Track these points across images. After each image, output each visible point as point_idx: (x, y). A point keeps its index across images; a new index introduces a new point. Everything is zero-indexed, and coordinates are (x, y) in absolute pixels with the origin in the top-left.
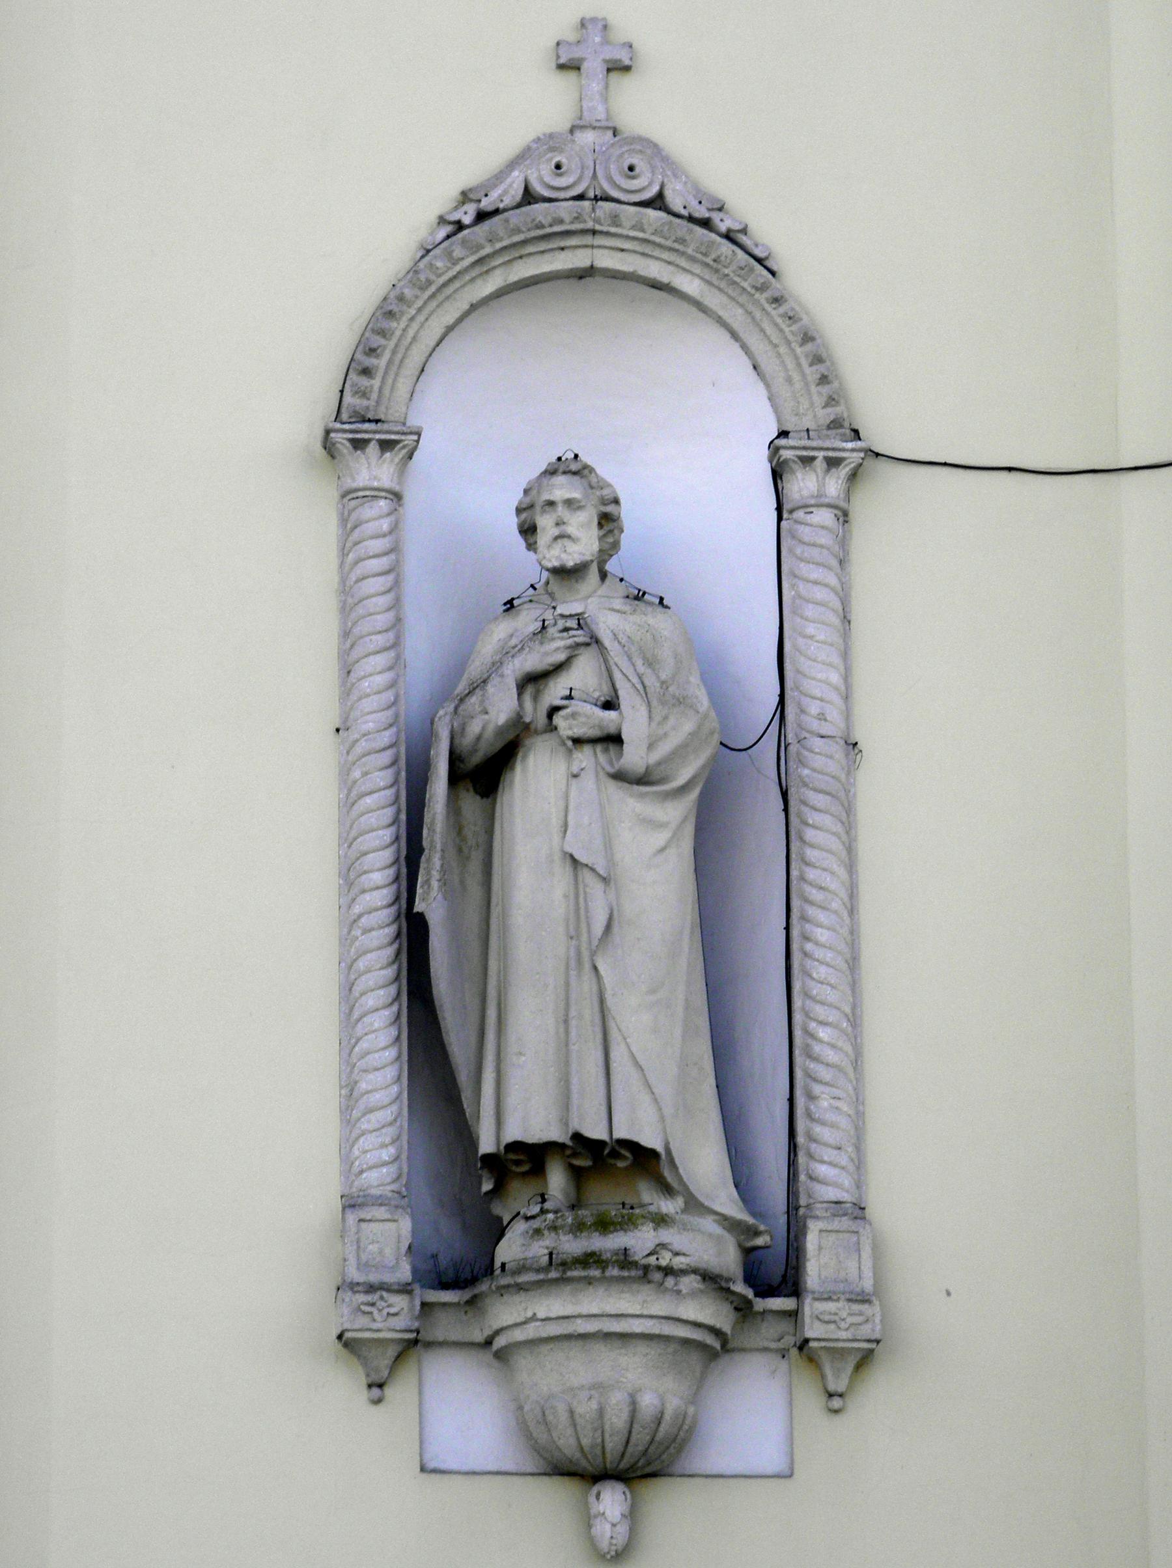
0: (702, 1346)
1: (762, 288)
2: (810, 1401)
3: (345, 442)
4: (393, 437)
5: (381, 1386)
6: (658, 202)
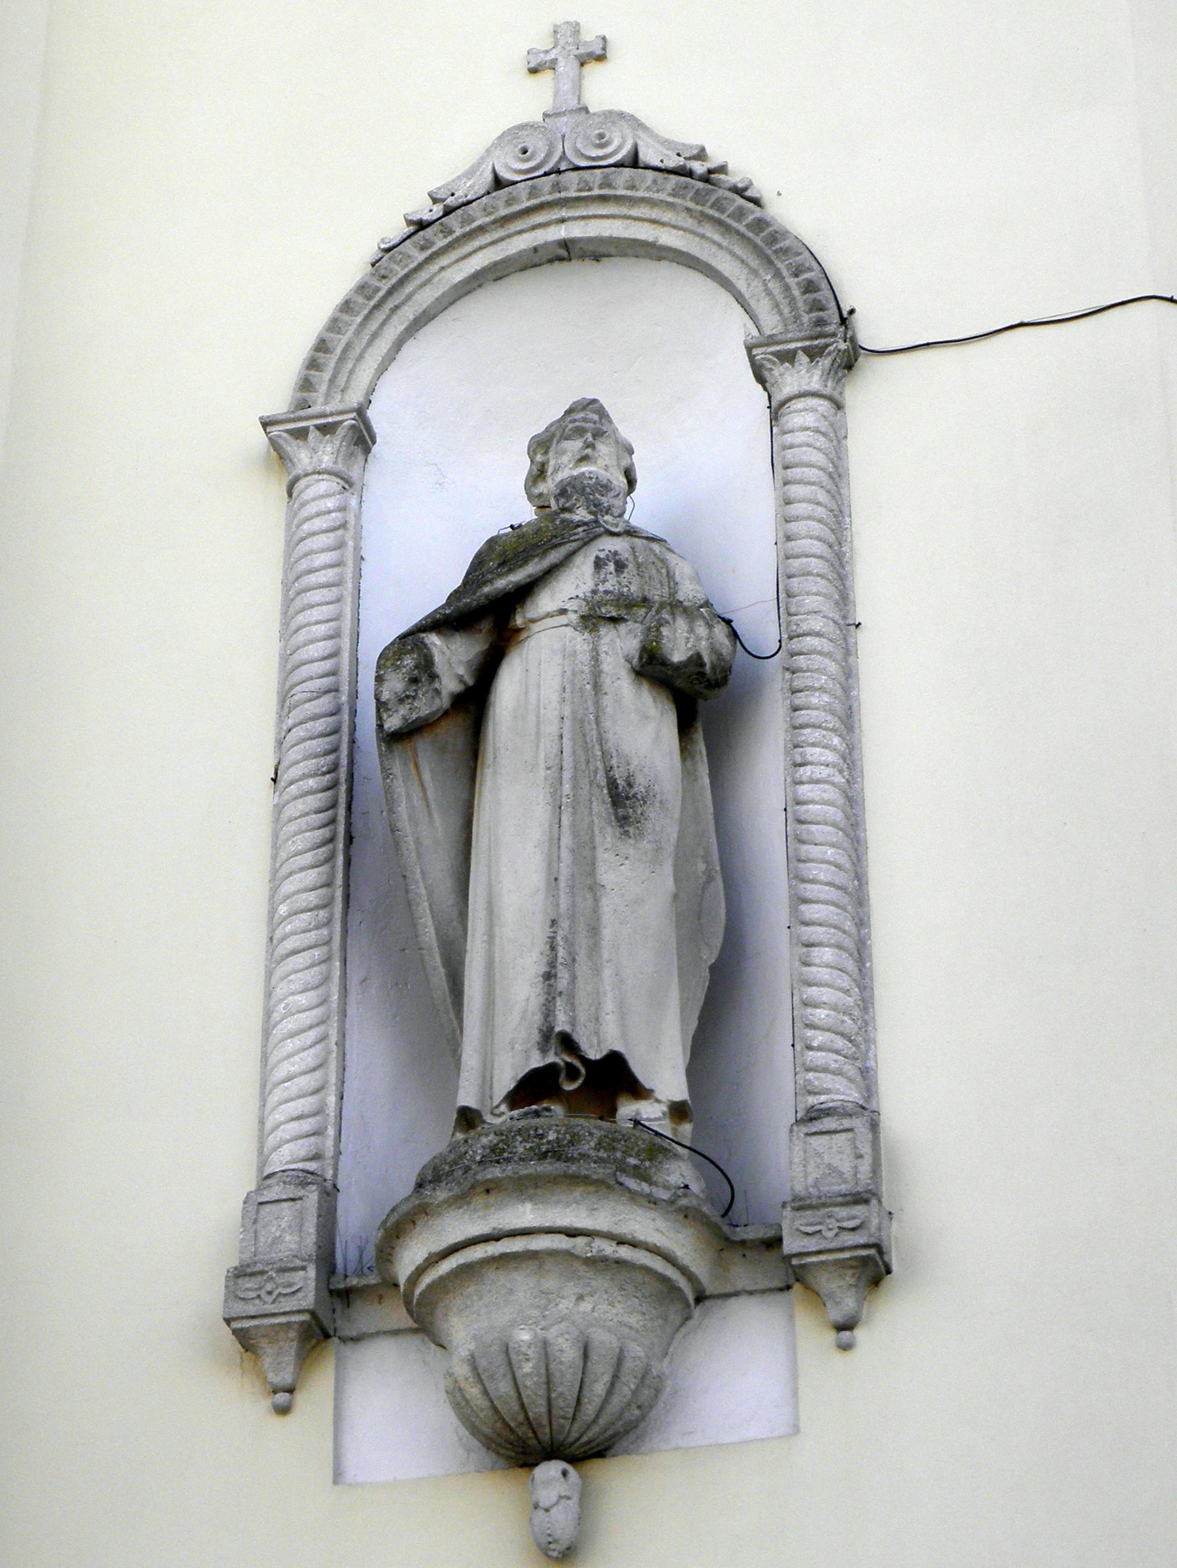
0: (669, 1289)
1: (740, 214)
2: (814, 1338)
3: (285, 435)
4: (330, 420)
5: (291, 1390)
6: (634, 161)
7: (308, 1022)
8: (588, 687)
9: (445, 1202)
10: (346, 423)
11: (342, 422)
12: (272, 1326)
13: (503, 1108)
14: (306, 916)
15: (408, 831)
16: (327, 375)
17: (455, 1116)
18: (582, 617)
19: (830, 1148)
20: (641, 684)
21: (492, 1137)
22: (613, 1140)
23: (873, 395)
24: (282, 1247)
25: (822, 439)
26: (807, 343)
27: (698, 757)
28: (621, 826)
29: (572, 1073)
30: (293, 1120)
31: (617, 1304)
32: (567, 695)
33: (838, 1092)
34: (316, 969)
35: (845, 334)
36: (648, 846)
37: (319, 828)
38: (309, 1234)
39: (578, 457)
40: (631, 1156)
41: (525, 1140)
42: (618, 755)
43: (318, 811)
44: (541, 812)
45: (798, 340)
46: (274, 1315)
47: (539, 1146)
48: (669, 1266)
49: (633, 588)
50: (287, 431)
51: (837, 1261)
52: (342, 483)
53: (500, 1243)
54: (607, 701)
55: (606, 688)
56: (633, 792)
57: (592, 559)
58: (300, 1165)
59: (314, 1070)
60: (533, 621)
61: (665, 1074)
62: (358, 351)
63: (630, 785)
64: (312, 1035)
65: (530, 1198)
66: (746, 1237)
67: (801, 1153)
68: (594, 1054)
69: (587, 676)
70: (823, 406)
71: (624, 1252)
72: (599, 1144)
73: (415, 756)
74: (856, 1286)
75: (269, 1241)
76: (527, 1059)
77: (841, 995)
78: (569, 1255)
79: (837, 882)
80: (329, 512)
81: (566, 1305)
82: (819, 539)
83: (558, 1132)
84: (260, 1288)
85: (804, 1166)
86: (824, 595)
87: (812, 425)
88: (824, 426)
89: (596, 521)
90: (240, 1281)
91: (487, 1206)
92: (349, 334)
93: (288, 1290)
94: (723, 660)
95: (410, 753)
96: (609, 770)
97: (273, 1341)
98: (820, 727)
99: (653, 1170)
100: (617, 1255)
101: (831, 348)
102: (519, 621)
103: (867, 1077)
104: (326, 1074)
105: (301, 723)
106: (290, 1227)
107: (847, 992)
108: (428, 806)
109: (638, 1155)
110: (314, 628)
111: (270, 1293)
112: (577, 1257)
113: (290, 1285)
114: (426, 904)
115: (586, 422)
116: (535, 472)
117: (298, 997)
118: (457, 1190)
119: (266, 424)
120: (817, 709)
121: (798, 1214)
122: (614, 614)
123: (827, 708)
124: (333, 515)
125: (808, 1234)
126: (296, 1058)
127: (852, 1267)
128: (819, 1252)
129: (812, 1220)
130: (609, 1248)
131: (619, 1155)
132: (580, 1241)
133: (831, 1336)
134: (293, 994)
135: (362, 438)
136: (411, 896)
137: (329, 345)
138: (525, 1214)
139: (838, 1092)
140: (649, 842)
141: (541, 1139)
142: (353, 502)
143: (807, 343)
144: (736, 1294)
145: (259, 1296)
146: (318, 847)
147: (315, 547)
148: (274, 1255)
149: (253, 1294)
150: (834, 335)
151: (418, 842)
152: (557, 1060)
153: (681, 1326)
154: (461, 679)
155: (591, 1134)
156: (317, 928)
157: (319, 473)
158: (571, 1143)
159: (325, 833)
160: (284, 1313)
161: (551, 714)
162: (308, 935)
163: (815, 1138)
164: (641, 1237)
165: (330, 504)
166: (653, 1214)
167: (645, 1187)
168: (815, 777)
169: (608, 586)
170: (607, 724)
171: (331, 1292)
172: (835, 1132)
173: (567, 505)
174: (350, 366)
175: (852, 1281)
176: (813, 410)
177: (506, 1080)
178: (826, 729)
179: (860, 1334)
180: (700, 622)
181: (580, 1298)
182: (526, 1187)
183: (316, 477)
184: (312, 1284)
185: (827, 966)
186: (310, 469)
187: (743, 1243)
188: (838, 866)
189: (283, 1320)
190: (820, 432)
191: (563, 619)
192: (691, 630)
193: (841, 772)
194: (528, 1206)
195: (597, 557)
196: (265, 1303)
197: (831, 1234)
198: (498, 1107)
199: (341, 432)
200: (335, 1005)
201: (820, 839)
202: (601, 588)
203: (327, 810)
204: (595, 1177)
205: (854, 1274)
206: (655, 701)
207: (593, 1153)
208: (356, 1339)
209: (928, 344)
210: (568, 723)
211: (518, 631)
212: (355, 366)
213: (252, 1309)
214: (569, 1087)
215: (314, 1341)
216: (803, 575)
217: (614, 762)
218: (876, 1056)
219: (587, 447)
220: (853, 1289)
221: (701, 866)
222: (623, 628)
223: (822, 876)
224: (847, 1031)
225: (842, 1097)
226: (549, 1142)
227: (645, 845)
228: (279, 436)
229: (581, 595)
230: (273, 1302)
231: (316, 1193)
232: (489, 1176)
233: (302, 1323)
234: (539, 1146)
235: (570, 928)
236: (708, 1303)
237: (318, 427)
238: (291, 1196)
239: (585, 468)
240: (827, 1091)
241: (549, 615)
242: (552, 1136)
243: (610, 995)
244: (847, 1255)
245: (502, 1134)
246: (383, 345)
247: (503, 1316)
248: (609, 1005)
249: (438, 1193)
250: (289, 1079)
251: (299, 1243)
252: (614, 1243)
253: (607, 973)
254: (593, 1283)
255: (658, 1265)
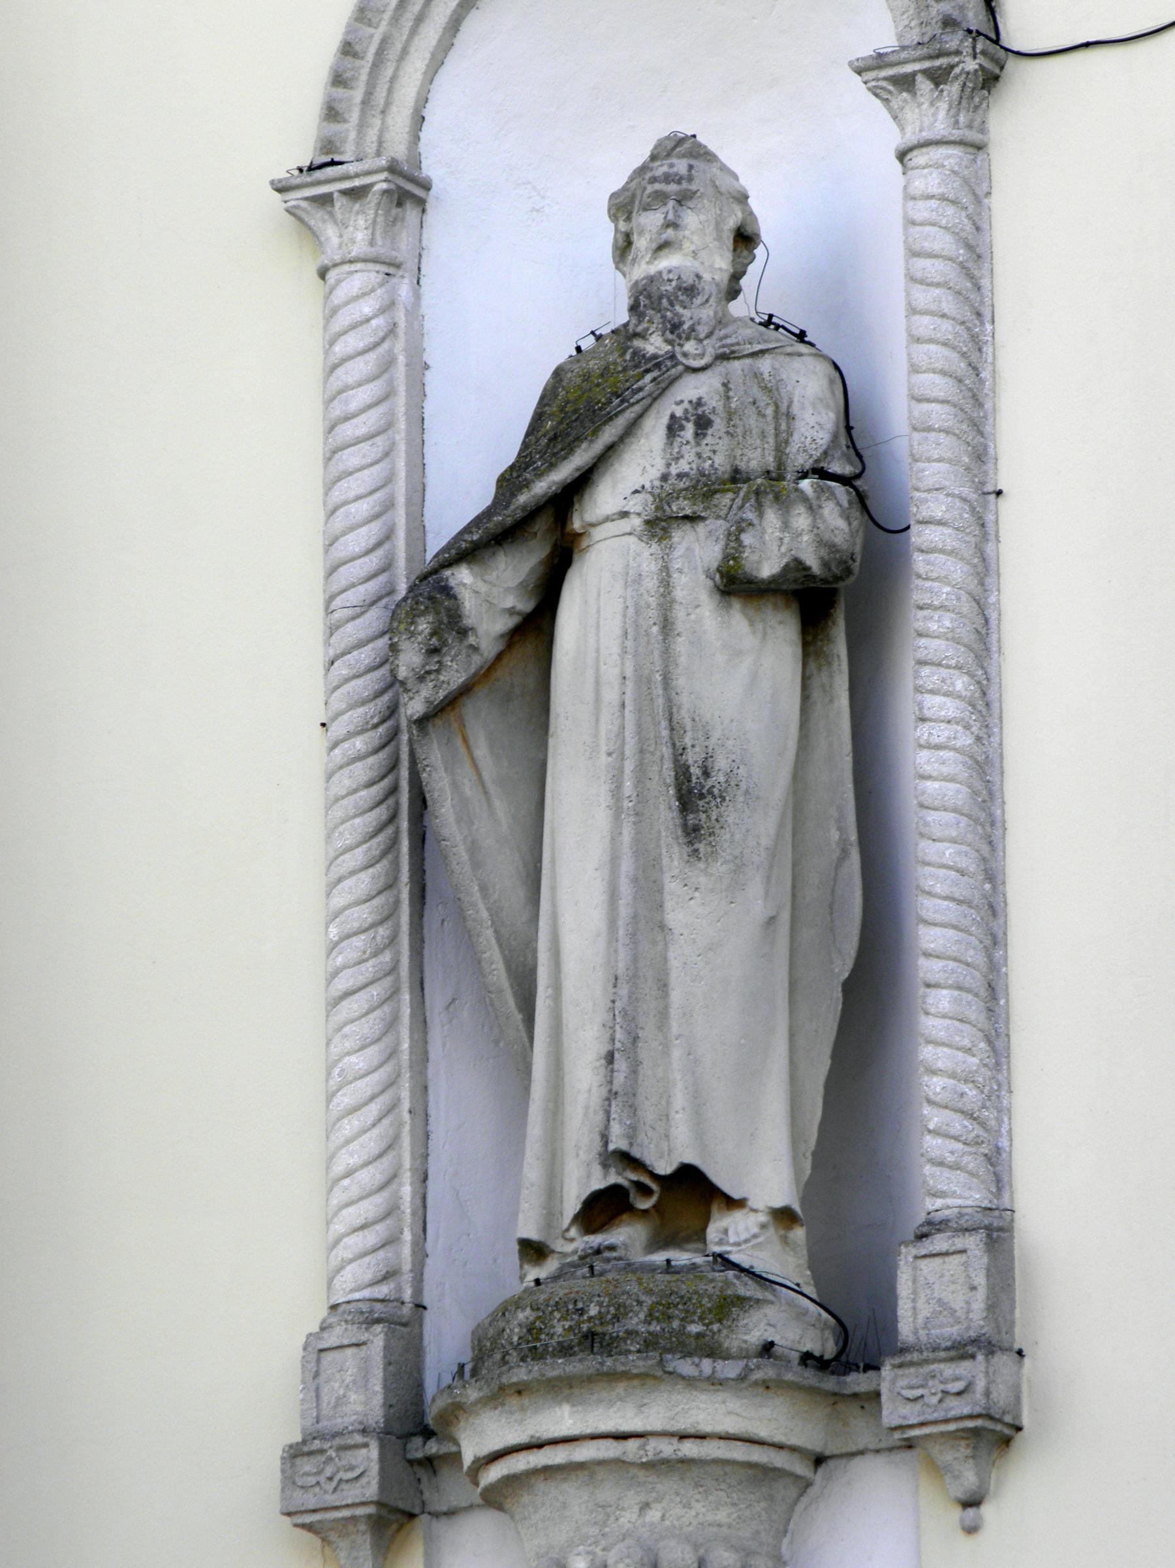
0: (763, 1474)
4: (357, 183)
7: (369, 1093)
8: (655, 629)
9: (478, 1401)
10: (377, 188)
11: (372, 185)
12: (336, 1520)
13: (573, 1232)
14: (358, 942)
15: (459, 838)
16: (358, 95)
17: (517, 1247)
18: (647, 522)
19: (942, 1276)
20: (729, 606)
21: (528, 1311)
22: (668, 1306)
23: (1034, 118)
24: (347, 1409)
25: (950, 210)
26: (927, 64)
27: (836, 664)
28: (690, 843)
29: (645, 1191)
30: (355, 1230)
31: (694, 1504)
32: (629, 644)
33: (953, 1195)
34: (378, 1013)
35: (974, 48)
36: (723, 869)
37: (372, 809)
38: (375, 1393)
39: (654, 246)
40: (693, 1322)
41: (563, 1318)
42: (694, 729)
43: (370, 784)
44: (602, 818)
45: (914, 61)
46: (336, 1508)
47: (578, 1324)
48: (756, 1448)
49: (719, 460)
50: (306, 199)
51: (943, 1434)
52: (385, 269)
53: (543, 1451)
54: (681, 645)
55: (680, 626)
56: (709, 783)
57: (665, 420)
58: (366, 1293)
59: (380, 1156)
60: (593, 525)
61: (763, 1169)
62: (399, 46)
63: (706, 774)
64: (374, 1109)
65: (568, 1399)
66: (857, 1389)
67: (910, 1283)
68: (664, 1168)
69: (653, 614)
70: (951, 156)
71: (690, 1449)
72: (650, 1315)
73: (462, 726)
74: (973, 1457)
75: (333, 1401)
76: (589, 1176)
77: (960, 1055)
78: (618, 1463)
79: (957, 895)
80: (368, 320)
81: (628, 1518)
82: (943, 373)
83: (600, 1304)
84: (319, 1473)
85: (914, 1301)
86: (950, 461)
87: (936, 191)
88: (953, 188)
89: (672, 357)
90: (298, 1461)
91: (523, 1409)
92: (383, 27)
93: (350, 1475)
94: (838, 551)
95: (455, 725)
96: (678, 753)
97: (343, 1535)
98: (939, 665)
99: (725, 1332)
100: (680, 1454)
101: (957, 70)
102: (577, 524)
103: (996, 1166)
104: (400, 1157)
105: (343, 654)
106: (354, 1382)
107: (968, 1051)
108: (486, 793)
109: (701, 1319)
110: (353, 508)
111: (330, 1479)
112: (632, 1464)
113: (352, 1468)
114: (490, 933)
115: (675, 176)
116: (621, 242)
117: (353, 1059)
118: (486, 1391)
119: (282, 188)
120: (938, 637)
121: (900, 1372)
122: (688, 512)
123: (950, 635)
124: (374, 322)
125: (908, 1399)
126: (354, 1146)
127: (963, 1438)
128: (922, 1424)
129: (914, 1382)
130: (667, 1448)
131: (676, 1324)
132: (632, 1444)
133: (956, 1513)
134: (348, 1054)
135: (408, 191)
136: (470, 923)
137: (358, 48)
138: (562, 1419)
139: (953, 1195)
140: (725, 862)
141: (581, 1315)
142: (404, 290)
143: (927, 64)
144: (861, 1453)
145: (318, 1483)
146: (372, 837)
147: (350, 381)
148: (339, 1420)
149: (312, 1480)
150: (958, 53)
151: (474, 848)
152: (620, 1180)
153: (801, 1495)
154: (511, 611)
155: (640, 1303)
156: (375, 955)
157: (351, 262)
158: (617, 1318)
159: (382, 813)
160: (348, 1506)
161: (611, 673)
162: (363, 967)
163: (926, 1261)
164: (707, 1428)
165: (367, 307)
166: (721, 1396)
167: (707, 1365)
168: (935, 740)
169: (683, 466)
170: (680, 681)
171: (411, 1462)
172: (947, 1254)
173: (639, 329)
174: (389, 72)
175: (969, 1452)
176: (939, 166)
177: (572, 1204)
178: (948, 667)
179: (987, 1510)
180: (800, 509)
181: (645, 1506)
182: (560, 1389)
183: (346, 268)
184: (375, 1468)
185: (944, 1016)
186: (337, 258)
187: (855, 1396)
188: (962, 872)
189: (346, 1513)
190: (947, 200)
191: (624, 525)
192: (786, 526)
193: (967, 727)
194: (566, 1408)
195: (673, 416)
196: (326, 1492)
197: (934, 1400)
198: (567, 1230)
199: (373, 198)
200: (405, 1057)
201: (937, 833)
202: (674, 470)
203: (383, 777)
204: (635, 1371)
205: (968, 1445)
206: (751, 623)
207: (642, 1328)
208: (450, 1513)
209: (1087, 45)
210: (630, 685)
211: (577, 536)
212: (397, 69)
213: (312, 1503)
214: (645, 1204)
215: (394, 1527)
216: (924, 430)
217: (688, 740)
218: (1010, 1132)
219: (668, 226)
220: (971, 1461)
221: (835, 835)
222: (701, 528)
223: (938, 889)
224: (968, 1107)
225: (959, 1202)
226: (590, 1319)
227: (719, 868)
228: (297, 207)
229: (648, 485)
230: (335, 1489)
231: (382, 1336)
232: (514, 1380)
233: (369, 1516)
234: (578, 1324)
235: (631, 994)
236: (832, 1464)
237: (344, 192)
238: (354, 1341)
239: (668, 262)
240: (943, 1194)
241: (608, 519)
242: (593, 1311)
243: (680, 1085)
244: (952, 1427)
245: (538, 1309)
246: (431, 33)
247: (561, 1534)
248: (679, 1100)
249: (469, 1391)
250: (349, 1174)
251: (366, 1404)
252: (675, 1440)
253: (676, 1053)
254: (659, 1486)
255: (739, 1452)
